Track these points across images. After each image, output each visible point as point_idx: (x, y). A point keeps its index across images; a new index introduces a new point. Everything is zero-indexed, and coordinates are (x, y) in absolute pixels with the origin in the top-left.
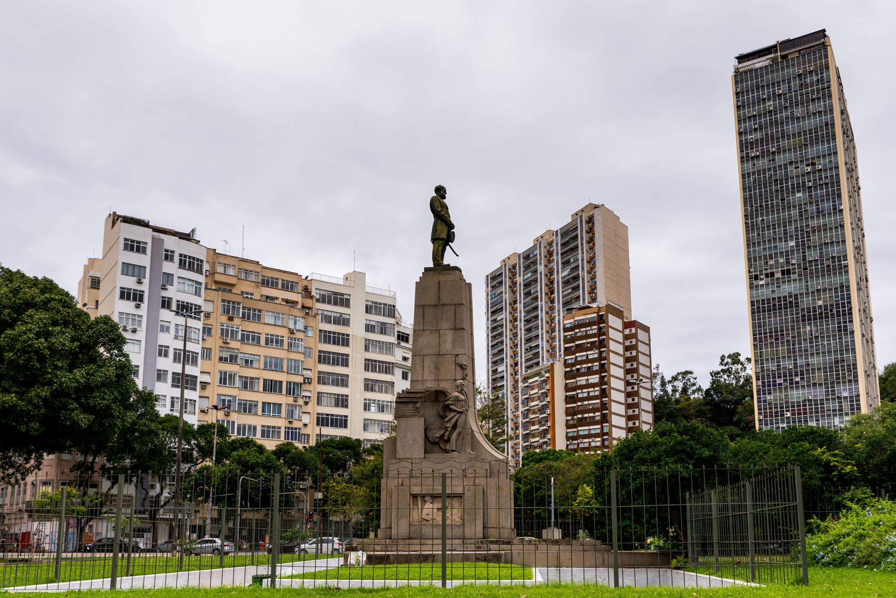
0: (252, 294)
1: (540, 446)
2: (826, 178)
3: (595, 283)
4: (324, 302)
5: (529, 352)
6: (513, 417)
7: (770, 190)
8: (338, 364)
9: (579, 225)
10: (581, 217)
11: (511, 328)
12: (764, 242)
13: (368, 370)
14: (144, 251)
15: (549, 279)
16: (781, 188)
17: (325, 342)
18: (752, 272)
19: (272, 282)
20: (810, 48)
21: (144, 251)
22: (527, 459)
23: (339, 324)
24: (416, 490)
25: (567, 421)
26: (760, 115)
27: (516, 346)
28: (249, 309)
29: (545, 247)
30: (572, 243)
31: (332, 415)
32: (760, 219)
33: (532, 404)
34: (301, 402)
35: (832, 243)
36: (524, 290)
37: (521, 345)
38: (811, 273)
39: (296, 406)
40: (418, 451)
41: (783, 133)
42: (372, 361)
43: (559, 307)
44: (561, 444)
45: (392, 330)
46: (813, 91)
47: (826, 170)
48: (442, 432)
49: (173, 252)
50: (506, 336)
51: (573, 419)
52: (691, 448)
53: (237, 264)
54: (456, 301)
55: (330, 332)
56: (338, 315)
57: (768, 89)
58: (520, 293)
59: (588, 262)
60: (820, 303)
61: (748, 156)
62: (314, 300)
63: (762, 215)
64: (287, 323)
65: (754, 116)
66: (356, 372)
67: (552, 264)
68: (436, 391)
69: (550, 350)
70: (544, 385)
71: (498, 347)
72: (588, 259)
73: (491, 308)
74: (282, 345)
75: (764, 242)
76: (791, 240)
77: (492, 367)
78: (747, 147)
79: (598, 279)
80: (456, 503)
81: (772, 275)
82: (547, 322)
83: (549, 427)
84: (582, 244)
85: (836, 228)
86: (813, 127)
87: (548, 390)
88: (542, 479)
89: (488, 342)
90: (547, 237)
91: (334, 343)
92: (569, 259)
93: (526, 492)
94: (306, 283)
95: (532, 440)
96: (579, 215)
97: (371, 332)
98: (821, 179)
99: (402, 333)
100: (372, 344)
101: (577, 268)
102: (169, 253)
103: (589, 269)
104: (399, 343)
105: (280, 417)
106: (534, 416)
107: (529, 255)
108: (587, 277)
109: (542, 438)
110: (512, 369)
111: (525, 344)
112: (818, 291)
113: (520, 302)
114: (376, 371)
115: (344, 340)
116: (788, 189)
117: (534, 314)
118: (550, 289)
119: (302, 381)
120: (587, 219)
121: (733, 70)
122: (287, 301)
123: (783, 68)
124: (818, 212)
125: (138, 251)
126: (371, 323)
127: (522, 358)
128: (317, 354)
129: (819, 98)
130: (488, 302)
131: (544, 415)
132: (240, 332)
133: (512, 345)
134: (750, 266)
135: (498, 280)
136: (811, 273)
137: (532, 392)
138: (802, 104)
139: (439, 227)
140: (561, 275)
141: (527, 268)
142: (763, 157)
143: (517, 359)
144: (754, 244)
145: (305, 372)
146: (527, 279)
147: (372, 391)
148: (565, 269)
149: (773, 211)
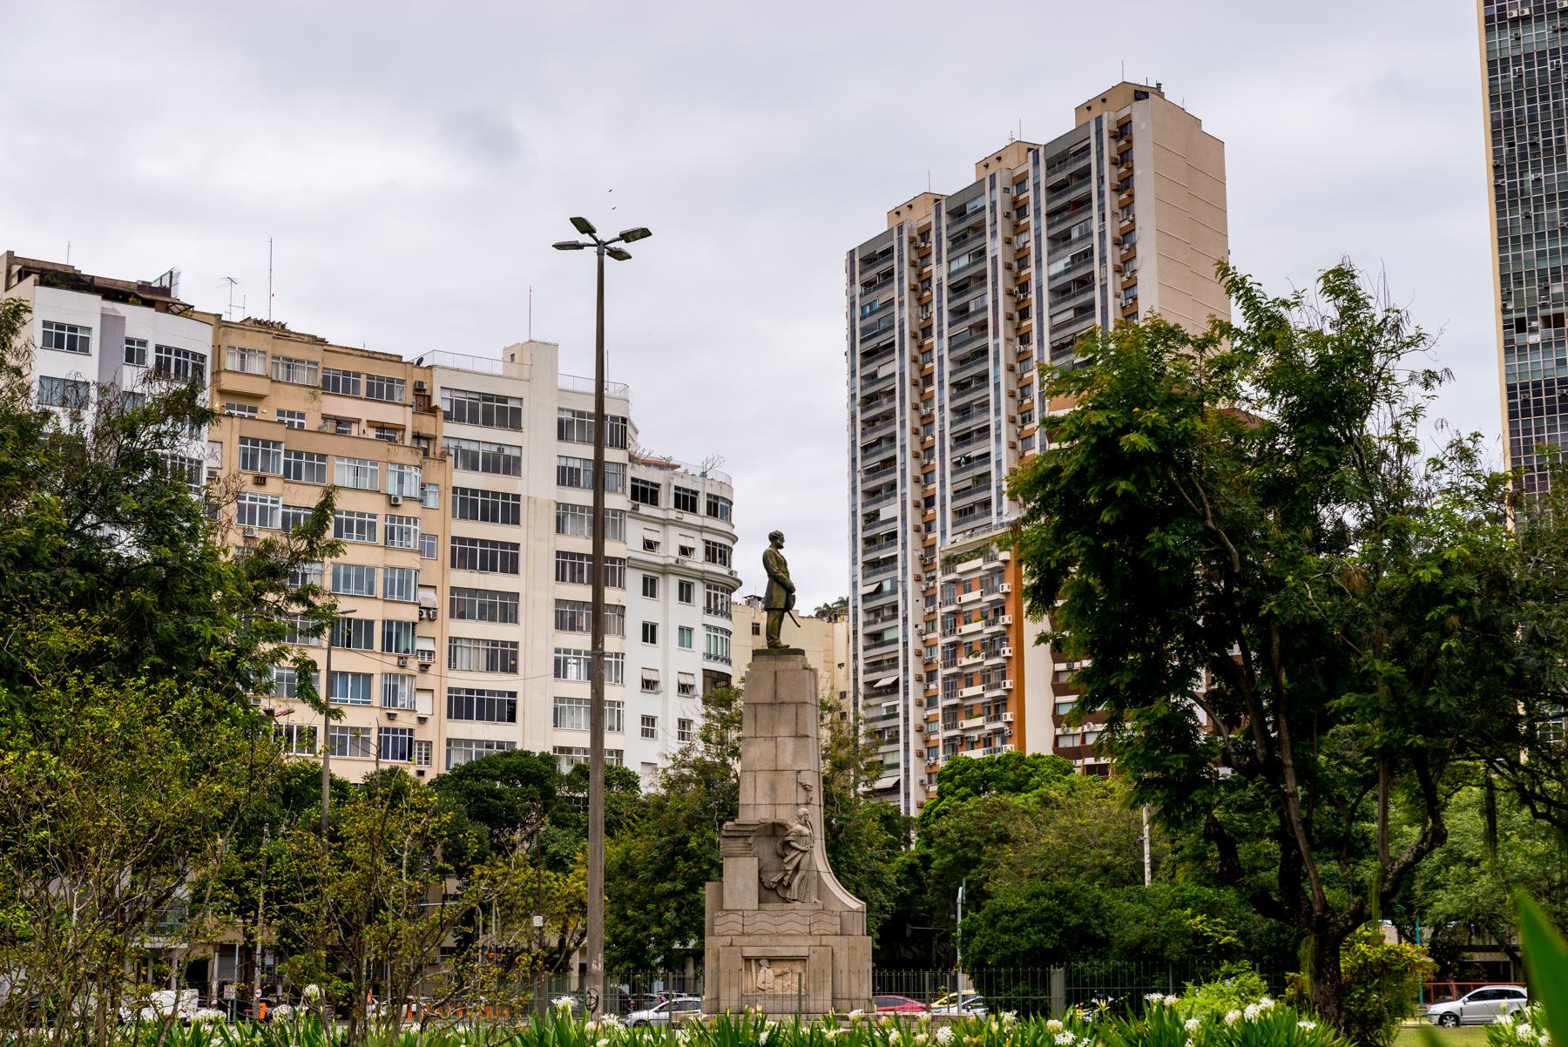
0: (301, 416)
1: (987, 742)
3: (1135, 299)
4: (460, 419)
5: (963, 470)
6: (920, 647)
8: (494, 569)
9: (1093, 141)
10: (1099, 120)
11: (917, 400)
12: (1541, 236)
13: (564, 580)
14: (85, 350)
15: (1017, 278)
17: (463, 516)
18: (1511, 311)
19: (346, 382)
21: (85, 350)
22: (951, 778)
23: (496, 471)
25: (1056, 674)
27: (929, 450)
28: (299, 455)
29: (1006, 190)
30: (1075, 188)
31: (481, 692)
32: (1531, 177)
33: (966, 629)
34: (413, 665)
36: (949, 301)
37: (942, 450)
39: (403, 677)
40: (751, 900)
42: (573, 555)
44: (1039, 739)
45: (620, 478)
48: (780, 876)
49: (143, 343)
50: (903, 423)
51: (1070, 670)
52: (1059, 914)
53: (268, 349)
54: (797, 698)
55: (475, 492)
56: (494, 449)
58: (940, 309)
59: (1118, 243)
61: (1502, 17)
62: (440, 416)
63: (1536, 169)
64: (384, 484)
67: (1024, 238)
68: (774, 824)
70: (996, 580)
72: (1118, 235)
73: (862, 341)
74: (373, 536)
75: (1541, 236)
77: (864, 506)
80: (798, 968)
82: (1012, 395)
83: (1009, 690)
84: (1101, 194)
87: (1007, 594)
88: (982, 840)
89: (855, 648)
90: (1010, 161)
91: (485, 519)
92: (1069, 230)
94: (418, 376)
95: (967, 724)
97: (571, 485)
99: (643, 482)
100: (573, 516)
101: (1087, 255)
102: (135, 347)
103: (1118, 262)
104: (635, 508)
105: (368, 704)
106: (971, 660)
107: (964, 206)
108: (1113, 283)
109: (989, 720)
110: (918, 513)
111: (952, 449)
113: (940, 334)
115: (507, 509)
118: (1018, 303)
119: (416, 619)
120: (1115, 128)
122: (381, 427)
125: (72, 347)
126: (571, 463)
127: (945, 484)
128: (449, 545)
130: (853, 327)
131: (997, 661)
132: (281, 510)
133: (918, 448)
134: (1506, 297)
137: (966, 598)
139: (775, 594)
140: (1048, 270)
141: (958, 241)
142: (1540, 19)
143: (930, 487)
144: (1516, 239)
145: (422, 593)
147: (572, 628)
148: (1058, 254)
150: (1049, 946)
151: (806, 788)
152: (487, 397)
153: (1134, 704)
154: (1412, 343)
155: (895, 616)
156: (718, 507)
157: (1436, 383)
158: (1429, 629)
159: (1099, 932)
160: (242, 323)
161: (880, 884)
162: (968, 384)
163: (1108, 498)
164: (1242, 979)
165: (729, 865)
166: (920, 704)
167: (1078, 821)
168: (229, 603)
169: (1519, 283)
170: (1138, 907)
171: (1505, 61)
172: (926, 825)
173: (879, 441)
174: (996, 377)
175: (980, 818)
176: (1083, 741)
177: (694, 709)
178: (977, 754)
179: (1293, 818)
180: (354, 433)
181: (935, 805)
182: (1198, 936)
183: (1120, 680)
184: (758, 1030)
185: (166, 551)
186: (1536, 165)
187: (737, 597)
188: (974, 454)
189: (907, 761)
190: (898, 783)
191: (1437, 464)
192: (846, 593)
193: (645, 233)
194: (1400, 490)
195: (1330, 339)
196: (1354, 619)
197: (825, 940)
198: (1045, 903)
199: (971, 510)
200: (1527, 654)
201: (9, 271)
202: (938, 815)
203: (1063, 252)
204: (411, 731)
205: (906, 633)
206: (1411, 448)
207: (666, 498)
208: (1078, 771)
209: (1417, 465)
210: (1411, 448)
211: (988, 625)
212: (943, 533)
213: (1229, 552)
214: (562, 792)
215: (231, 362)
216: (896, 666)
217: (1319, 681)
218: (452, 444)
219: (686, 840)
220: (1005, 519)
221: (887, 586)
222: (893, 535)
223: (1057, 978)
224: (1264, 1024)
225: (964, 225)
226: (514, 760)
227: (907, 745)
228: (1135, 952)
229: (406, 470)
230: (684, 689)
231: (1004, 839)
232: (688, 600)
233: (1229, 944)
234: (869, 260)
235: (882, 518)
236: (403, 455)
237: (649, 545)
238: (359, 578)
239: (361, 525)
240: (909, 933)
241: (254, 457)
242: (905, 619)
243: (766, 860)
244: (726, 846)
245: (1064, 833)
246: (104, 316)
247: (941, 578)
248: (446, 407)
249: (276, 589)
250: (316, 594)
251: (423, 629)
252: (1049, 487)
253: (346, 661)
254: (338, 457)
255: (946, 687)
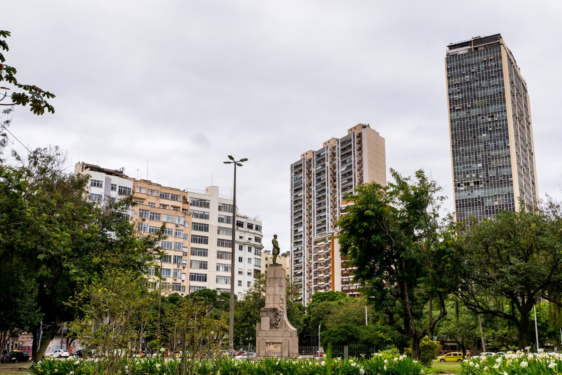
0: (155, 204)
1: (325, 288)
2: (500, 126)
3: (363, 177)
4: (194, 205)
6: (308, 264)
7: (467, 131)
8: (202, 243)
10: (354, 133)
11: (308, 202)
12: (464, 163)
14: (101, 187)
15: (333, 172)
16: (474, 130)
17: (194, 230)
19: (166, 196)
20: (491, 44)
21: (101, 187)
22: (316, 297)
23: (203, 218)
24: (267, 341)
25: (342, 271)
26: (461, 84)
27: (311, 214)
28: (154, 214)
29: (331, 150)
31: (198, 274)
32: (461, 148)
33: (320, 259)
34: (181, 267)
35: (503, 166)
36: (316, 177)
37: (314, 214)
38: (491, 185)
39: (178, 270)
40: (268, 328)
41: (475, 96)
42: (222, 240)
43: (339, 192)
44: (338, 288)
46: (492, 71)
47: (500, 121)
49: (116, 185)
50: (304, 208)
51: (346, 270)
54: (280, 277)
55: (197, 224)
56: (203, 213)
57: (466, 68)
58: (314, 179)
59: (358, 163)
60: (497, 203)
61: (454, 109)
62: (189, 204)
63: (462, 146)
64: (175, 221)
65: (458, 84)
66: (212, 247)
67: (335, 162)
69: (333, 219)
71: (298, 215)
75: (464, 163)
76: (480, 163)
78: (453, 103)
79: (364, 175)
80: (280, 345)
81: (468, 184)
82: (332, 201)
84: (354, 151)
85: (506, 157)
86: (492, 94)
87: (330, 251)
88: (324, 313)
89: (291, 264)
90: (332, 143)
91: (200, 230)
92: (346, 160)
93: (314, 321)
94: (184, 194)
95: (320, 283)
96: (353, 131)
98: (497, 126)
101: (351, 166)
106: (321, 267)
107: (320, 154)
108: (357, 173)
109: (325, 283)
110: (308, 230)
111: (316, 214)
112: (495, 196)
113: (314, 185)
114: (224, 246)
115: (206, 228)
116: (477, 131)
117: (323, 194)
120: (358, 135)
121: (446, 54)
122: (174, 207)
123: (475, 56)
124: (495, 147)
125: (98, 186)
126: (222, 217)
127: (314, 223)
128: (191, 237)
129: (496, 77)
130: (292, 183)
131: (327, 268)
133: (308, 214)
134: (455, 178)
135: (300, 169)
136: (491, 185)
137: (320, 252)
138: (486, 79)
139: (275, 250)
140: (340, 170)
141: (318, 162)
142: (463, 110)
144: (457, 164)
145: (184, 249)
146: (319, 170)
149: (469, 144)
150: (343, 340)
151: (282, 299)
152: (201, 200)
153: (368, 279)
154: (438, 189)
155: (302, 256)
156: (258, 228)
157: (444, 199)
158: (443, 261)
159: (356, 337)
160: (140, 180)
161: (299, 324)
162: (321, 198)
163: (361, 227)
164: (393, 349)
165: (262, 319)
166: (308, 278)
167: (348, 308)
168: (139, 251)
169: (458, 175)
170: (366, 331)
171: (455, 120)
172: (309, 309)
173: (298, 212)
174: (328, 196)
175: (323, 308)
176: (349, 288)
177: (252, 279)
178: (322, 291)
179: (408, 308)
180: (168, 208)
181: (311, 304)
182: (381, 338)
183: (364, 273)
184: (276, 361)
185: (123, 237)
186: (462, 145)
187: (262, 251)
188: (322, 216)
189: (304, 293)
190: (302, 298)
191: (444, 219)
192: (289, 250)
193: (246, 160)
194: (435, 227)
195: (417, 188)
196: (424, 258)
197: (286, 338)
198: (343, 329)
199: (321, 229)
200: (467, 268)
201: (83, 167)
202: (312, 307)
203: (345, 165)
204: (180, 284)
205: (304, 260)
206: (437, 216)
207: (245, 226)
208: (348, 296)
209: (439, 220)
210: (437, 216)
211: (326, 258)
212: (314, 235)
213: (392, 241)
214: (218, 299)
215: (137, 190)
216: (302, 269)
217: (414, 274)
218: (192, 211)
219: (250, 312)
220: (330, 232)
221: (300, 248)
222: (301, 236)
223: (346, 349)
224: (404, 361)
225: (320, 158)
226: (206, 291)
227: (304, 289)
228: (366, 342)
229: (180, 218)
230: (249, 274)
231: (329, 313)
232: (250, 251)
233: (389, 340)
234: (296, 167)
235: (299, 231)
236: (180, 214)
237: (241, 237)
238: (168, 245)
239: (169, 231)
240: (305, 336)
241: (142, 214)
242: (304, 257)
243: (272, 318)
244: (261, 314)
245: (345, 311)
246: (106, 178)
247: (313, 247)
248: (191, 202)
249: (150, 248)
250: (160, 249)
251: (184, 258)
252: (347, 224)
253: (166, 266)
254: (164, 214)
255: (314, 274)
